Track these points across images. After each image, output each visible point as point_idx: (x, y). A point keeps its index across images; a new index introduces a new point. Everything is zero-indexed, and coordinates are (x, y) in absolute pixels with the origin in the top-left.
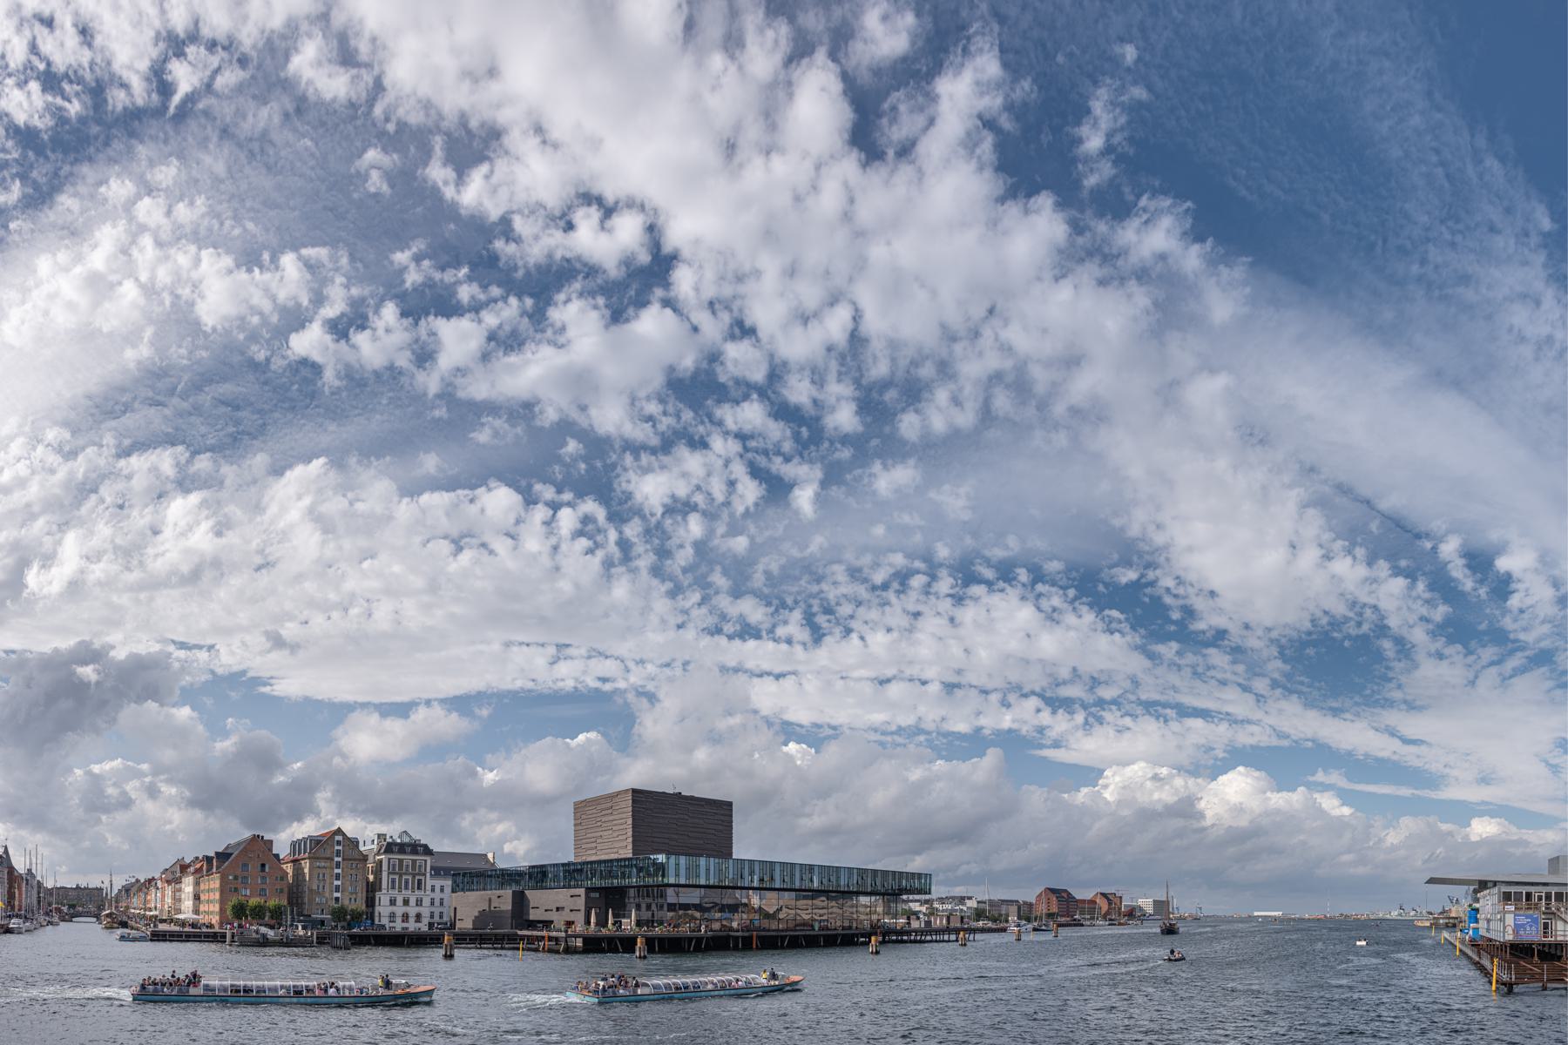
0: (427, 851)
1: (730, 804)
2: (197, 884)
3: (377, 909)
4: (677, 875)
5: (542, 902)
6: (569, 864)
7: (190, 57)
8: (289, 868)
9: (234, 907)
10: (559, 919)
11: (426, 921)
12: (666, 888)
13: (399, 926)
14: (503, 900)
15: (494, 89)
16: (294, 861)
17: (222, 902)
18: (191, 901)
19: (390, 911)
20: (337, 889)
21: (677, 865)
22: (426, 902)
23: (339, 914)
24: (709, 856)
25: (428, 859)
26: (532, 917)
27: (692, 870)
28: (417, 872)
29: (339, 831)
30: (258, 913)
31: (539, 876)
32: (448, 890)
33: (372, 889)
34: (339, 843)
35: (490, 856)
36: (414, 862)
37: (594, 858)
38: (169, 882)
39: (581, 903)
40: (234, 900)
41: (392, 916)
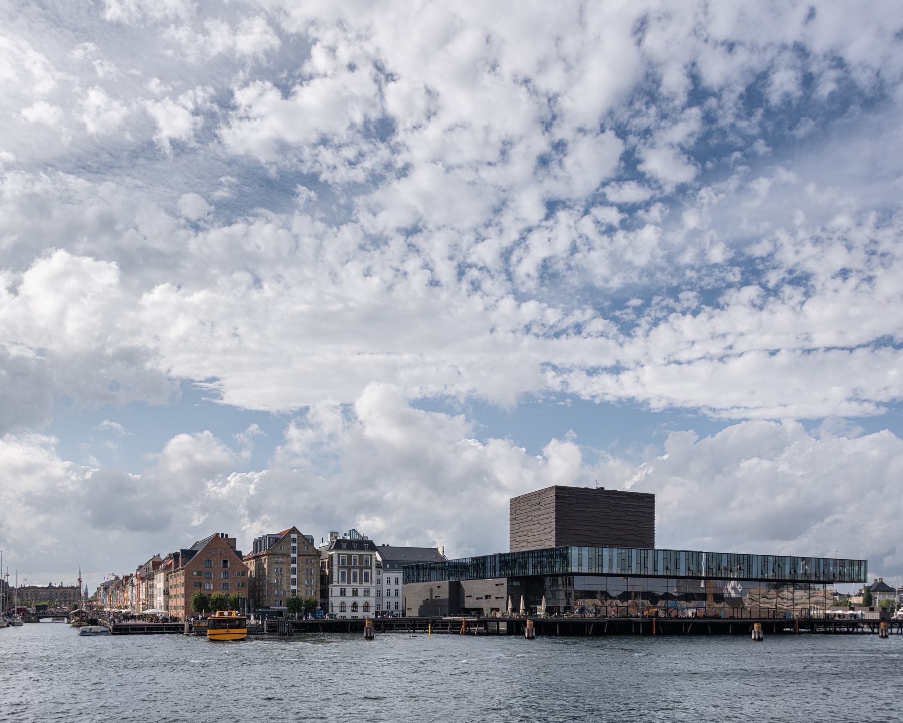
0: (372, 547)
1: (651, 497)
2: (167, 580)
3: (331, 599)
4: (581, 565)
5: (475, 591)
6: (504, 555)
8: (251, 566)
9: (195, 602)
10: (486, 606)
11: (373, 610)
12: (586, 572)
13: (349, 614)
14: (441, 589)
16: (257, 558)
17: (186, 596)
18: (162, 597)
19: (342, 601)
20: (294, 583)
21: (581, 555)
22: (373, 592)
23: (295, 604)
24: (611, 546)
26: (466, 605)
27: (596, 561)
28: (365, 565)
29: (294, 530)
30: (221, 604)
31: (479, 567)
32: (401, 582)
33: (325, 581)
34: (294, 540)
35: (441, 551)
36: (361, 556)
37: (525, 549)
38: (143, 579)
39: (503, 591)
40: (196, 594)
41: (343, 607)
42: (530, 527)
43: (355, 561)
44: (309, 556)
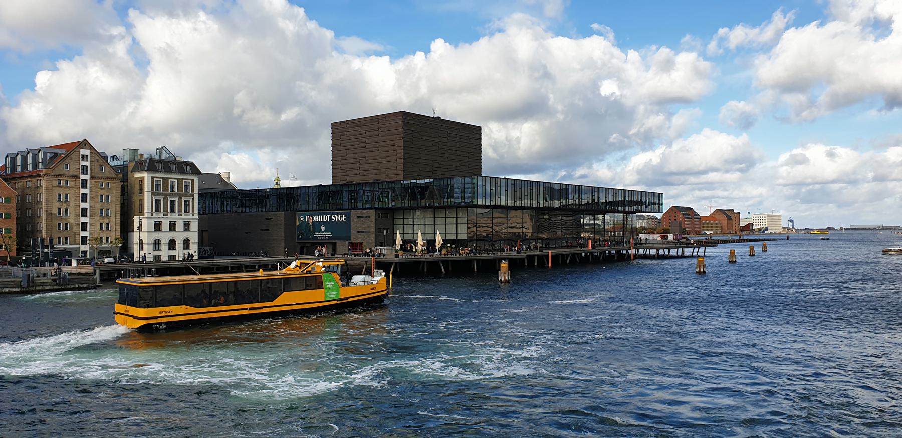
0: (194, 170)
1: (478, 129)
7: (434, 55)
15: (606, 165)
21: (538, 202)
25: (196, 179)
36: (166, 180)
42: (364, 154)
43: (173, 186)
44: (106, 178)
